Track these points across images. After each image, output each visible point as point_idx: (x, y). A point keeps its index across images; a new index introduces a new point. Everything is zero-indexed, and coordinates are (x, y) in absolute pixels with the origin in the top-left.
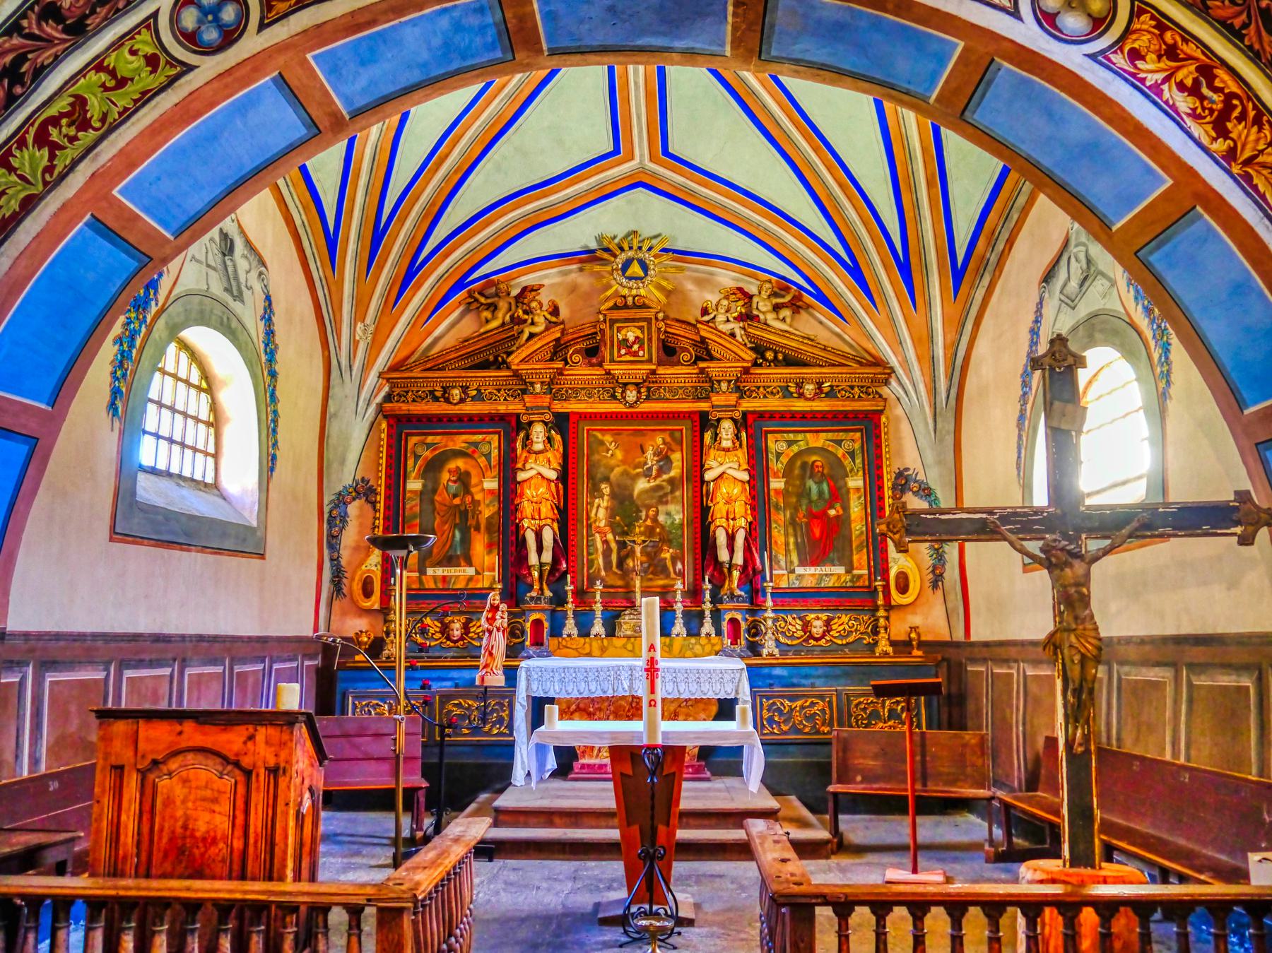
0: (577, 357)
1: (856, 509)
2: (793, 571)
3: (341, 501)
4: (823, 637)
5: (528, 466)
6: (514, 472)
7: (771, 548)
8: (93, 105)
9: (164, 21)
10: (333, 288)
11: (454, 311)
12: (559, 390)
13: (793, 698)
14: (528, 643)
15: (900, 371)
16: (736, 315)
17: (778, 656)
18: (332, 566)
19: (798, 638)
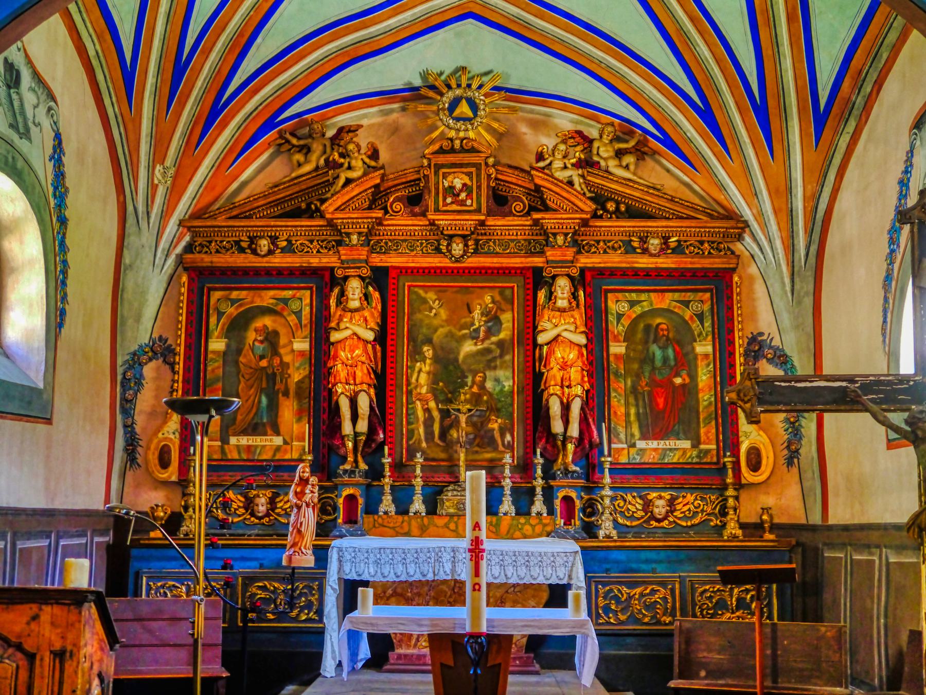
0: (398, 206)
1: (704, 378)
2: (634, 445)
5: (342, 326)
7: (609, 420)
10: (130, 127)
12: (378, 242)
13: (632, 585)
14: (340, 521)
16: (574, 161)
17: (616, 538)
18: (125, 433)
19: (639, 519)
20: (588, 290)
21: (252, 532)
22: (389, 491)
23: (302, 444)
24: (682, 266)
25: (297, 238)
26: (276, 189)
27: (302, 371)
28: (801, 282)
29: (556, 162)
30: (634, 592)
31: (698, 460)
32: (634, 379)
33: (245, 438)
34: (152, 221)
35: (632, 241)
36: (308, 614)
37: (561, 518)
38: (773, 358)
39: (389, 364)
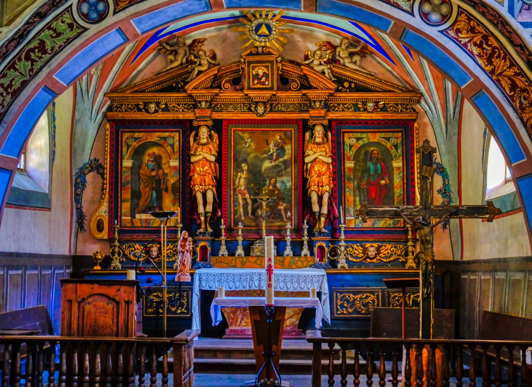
0: (227, 85)
1: (397, 180)
3: (82, 173)
4: (375, 257)
5: (197, 153)
6: (189, 156)
8: (47, 44)
9: (74, 9)
11: (149, 54)
12: (216, 105)
13: (355, 293)
16: (325, 60)
17: (347, 268)
18: (77, 213)
19: (360, 258)
27: (175, 178)
29: (316, 61)
33: (144, 215)
35: (358, 104)
36: (181, 310)
39: (223, 174)
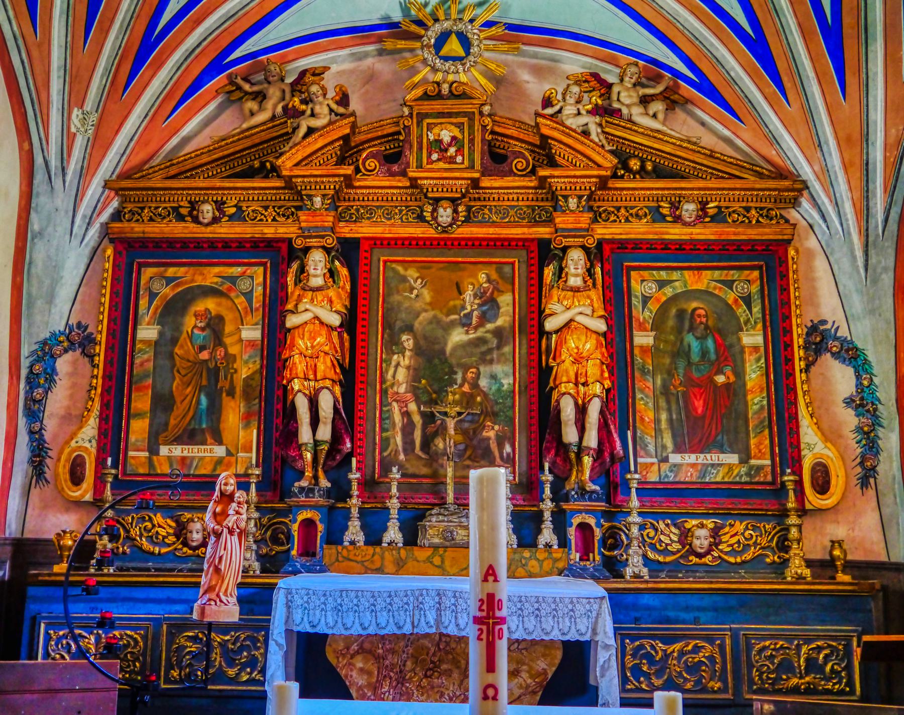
0: (372, 163)
1: (754, 376)
2: (665, 460)
4: (708, 552)
5: (301, 307)
7: (635, 427)
10: (35, 53)
12: (348, 208)
13: (669, 640)
14: (294, 553)
15: (816, 186)
16: (589, 107)
17: (647, 578)
18: (31, 441)
19: (674, 553)
20: (607, 267)
21: (184, 566)
22: (357, 515)
23: (248, 455)
24: (723, 237)
25: (249, 203)
26: (223, 143)
27: (251, 366)
28: (877, 255)
29: (568, 107)
30: (672, 649)
31: (748, 479)
32: (665, 376)
33: (179, 447)
34: (68, 178)
35: (660, 206)
36: (250, 673)
37: (577, 551)
38: (839, 352)
39: (359, 357)
